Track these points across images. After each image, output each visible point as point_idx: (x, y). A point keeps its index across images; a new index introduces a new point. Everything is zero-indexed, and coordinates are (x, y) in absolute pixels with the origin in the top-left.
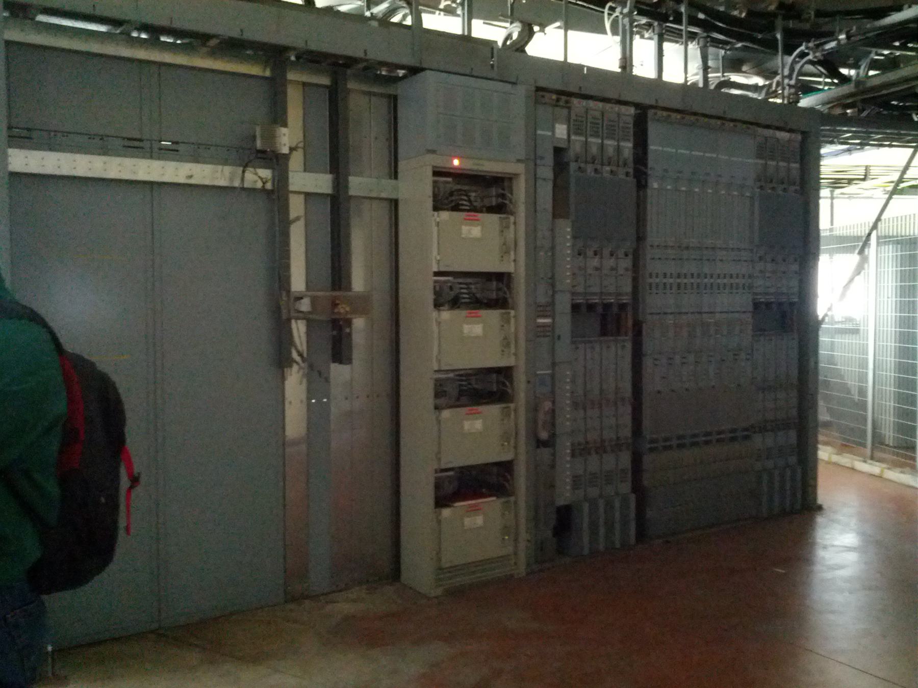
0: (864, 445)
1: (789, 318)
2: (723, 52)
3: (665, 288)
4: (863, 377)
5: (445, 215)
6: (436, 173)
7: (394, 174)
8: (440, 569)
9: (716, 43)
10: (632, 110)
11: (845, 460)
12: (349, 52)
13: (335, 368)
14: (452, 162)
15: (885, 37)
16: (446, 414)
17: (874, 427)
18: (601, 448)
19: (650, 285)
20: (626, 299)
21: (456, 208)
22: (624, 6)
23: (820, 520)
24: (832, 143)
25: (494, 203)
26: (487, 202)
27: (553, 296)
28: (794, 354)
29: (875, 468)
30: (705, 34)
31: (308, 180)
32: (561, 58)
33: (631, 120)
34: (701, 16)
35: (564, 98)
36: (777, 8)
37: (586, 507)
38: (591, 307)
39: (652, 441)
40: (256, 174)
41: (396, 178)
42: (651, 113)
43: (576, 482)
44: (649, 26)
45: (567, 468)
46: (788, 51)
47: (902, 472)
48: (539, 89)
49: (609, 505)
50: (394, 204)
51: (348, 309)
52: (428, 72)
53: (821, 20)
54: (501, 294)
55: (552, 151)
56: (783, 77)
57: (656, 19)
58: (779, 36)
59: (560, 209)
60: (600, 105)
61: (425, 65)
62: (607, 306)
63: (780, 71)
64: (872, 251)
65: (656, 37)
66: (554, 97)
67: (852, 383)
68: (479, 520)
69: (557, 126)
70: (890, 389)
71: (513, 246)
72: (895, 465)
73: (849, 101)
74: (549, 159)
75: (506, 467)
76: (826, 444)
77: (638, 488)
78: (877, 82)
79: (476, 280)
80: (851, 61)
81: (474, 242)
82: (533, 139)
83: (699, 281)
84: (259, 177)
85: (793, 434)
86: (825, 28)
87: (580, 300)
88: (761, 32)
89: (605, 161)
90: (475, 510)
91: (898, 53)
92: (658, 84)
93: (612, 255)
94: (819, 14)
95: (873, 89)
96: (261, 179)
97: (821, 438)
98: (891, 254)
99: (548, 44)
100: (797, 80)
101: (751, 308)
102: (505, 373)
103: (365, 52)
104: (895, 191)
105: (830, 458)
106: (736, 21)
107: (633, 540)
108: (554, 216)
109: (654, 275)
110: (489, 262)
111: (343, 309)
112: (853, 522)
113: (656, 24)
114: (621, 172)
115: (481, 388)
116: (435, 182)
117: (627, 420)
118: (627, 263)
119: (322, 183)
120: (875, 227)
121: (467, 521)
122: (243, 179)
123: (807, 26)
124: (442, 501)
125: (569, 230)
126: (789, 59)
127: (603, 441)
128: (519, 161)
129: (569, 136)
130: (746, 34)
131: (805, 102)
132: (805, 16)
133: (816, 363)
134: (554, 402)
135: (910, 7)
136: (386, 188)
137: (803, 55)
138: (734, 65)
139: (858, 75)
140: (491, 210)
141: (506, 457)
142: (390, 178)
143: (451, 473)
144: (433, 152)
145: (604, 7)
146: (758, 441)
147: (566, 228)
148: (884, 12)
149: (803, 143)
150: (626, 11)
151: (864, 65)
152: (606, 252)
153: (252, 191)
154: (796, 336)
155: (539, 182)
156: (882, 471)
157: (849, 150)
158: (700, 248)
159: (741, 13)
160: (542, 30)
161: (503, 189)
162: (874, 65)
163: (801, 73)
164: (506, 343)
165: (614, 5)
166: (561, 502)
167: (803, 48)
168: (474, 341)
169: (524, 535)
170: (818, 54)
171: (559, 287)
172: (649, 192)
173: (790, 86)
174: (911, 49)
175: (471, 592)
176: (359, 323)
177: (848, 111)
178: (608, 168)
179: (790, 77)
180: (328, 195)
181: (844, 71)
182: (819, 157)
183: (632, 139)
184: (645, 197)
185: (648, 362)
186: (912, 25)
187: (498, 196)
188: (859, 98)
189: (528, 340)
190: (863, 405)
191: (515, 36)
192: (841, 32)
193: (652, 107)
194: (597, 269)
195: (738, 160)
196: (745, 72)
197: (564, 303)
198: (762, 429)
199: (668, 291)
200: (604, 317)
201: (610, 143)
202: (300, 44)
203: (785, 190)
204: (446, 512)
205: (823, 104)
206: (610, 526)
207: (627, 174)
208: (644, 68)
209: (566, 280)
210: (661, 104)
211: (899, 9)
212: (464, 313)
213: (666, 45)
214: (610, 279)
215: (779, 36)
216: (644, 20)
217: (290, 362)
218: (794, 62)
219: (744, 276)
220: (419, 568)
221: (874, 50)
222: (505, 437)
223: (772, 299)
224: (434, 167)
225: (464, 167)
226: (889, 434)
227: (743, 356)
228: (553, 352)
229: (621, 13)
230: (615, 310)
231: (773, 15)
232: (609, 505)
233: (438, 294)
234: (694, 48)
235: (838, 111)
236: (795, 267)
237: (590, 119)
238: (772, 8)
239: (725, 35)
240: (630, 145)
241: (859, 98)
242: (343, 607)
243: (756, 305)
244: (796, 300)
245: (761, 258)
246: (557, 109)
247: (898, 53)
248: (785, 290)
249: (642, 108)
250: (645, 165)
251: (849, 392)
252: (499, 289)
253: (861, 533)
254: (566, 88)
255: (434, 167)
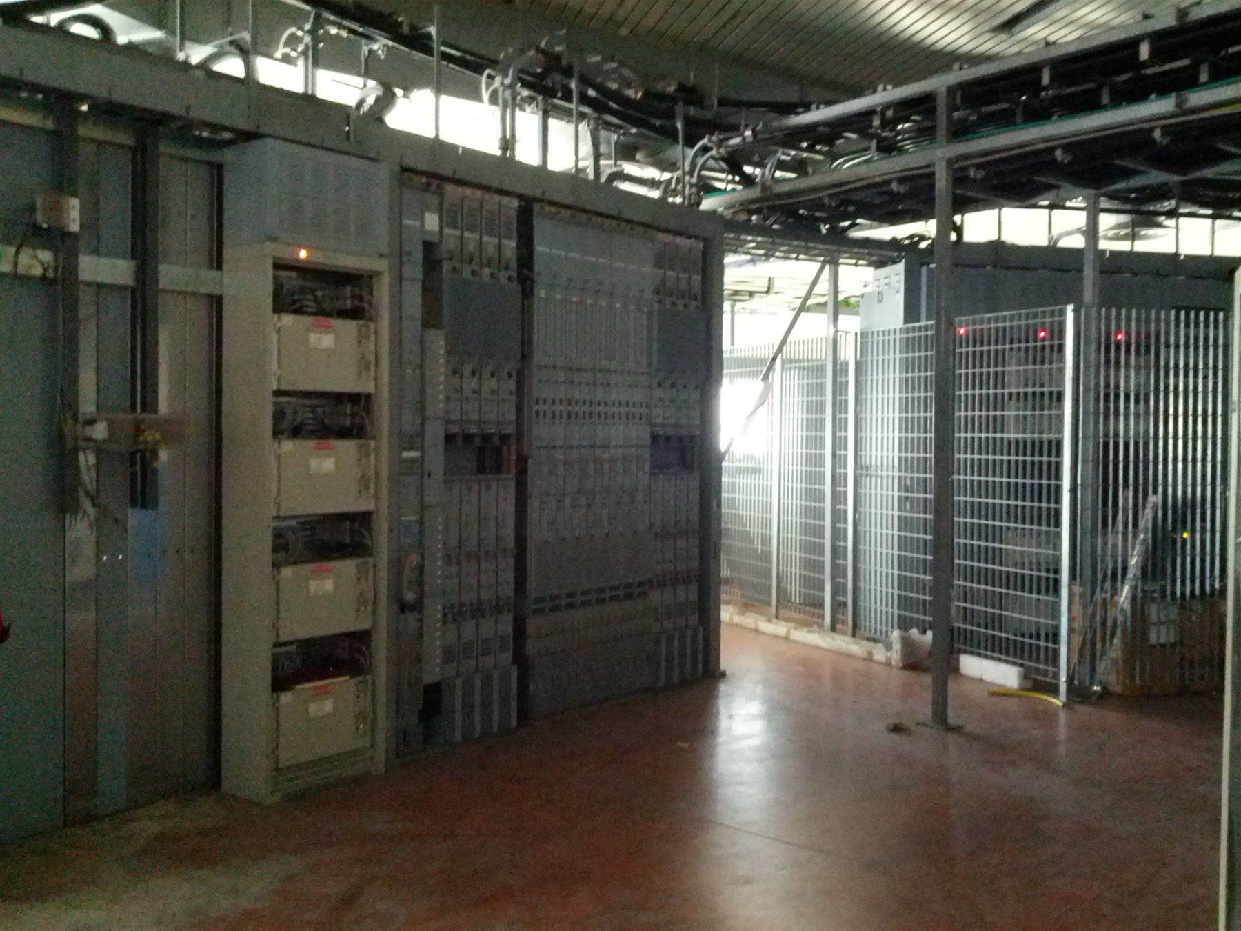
0: (769, 604)
1: (688, 454)
2: (615, 137)
3: (569, 417)
4: (767, 524)
5: (287, 320)
6: (277, 266)
7: (217, 262)
8: (277, 769)
9: (608, 126)
10: (515, 203)
11: (749, 620)
12: (161, 106)
13: (135, 518)
14: (298, 254)
15: (792, 137)
16: (287, 572)
17: (778, 582)
18: (477, 611)
19: (538, 412)
20: (510, 430)
21: (298, 311)
22: (506, 75)
23: (723, 688)
24: (735, 252)
25: (349, 307)
26: (338, 304)
27: (422, 424)
28: (695, 496)
29: (780, 628)
30: (595, 115)
31: (105, 268)
32: (431, 135)
33: (513, 214)
34: (591, 93)
35: (435, 182)
36: (677, 90)
37: (459, 683)
38: (468, 438)
39: (536, 601)
40: (35, 257)
41: (219, 267)
42: (536, 207)
43: (449, 655)
44: (531, 99)
45: (437, 639)
46: (690, 141)
47: (809, 632)
48: (405, 169)
49: (487, 679)
50: (216, 303)
51: (158, 436)
52: (269, 141)
53: (724, 110)
54: (357, 420)
55: (421, 247)
56: (684, 174)
57: (540, 93)
58: (679, 125)
59: (431, 319)
60: (478, 193)
61: (263, 130)
62: (487, 438)
63: (679, 164)
64: (776, 377)
65: (540, 113)
66: (424, 180)
67: (755, 531)
68: (328, 706)
69: (427, 215)
70: (796, 536)
71: (373, 363)
72: (801, 624)
73: (754, 207)
74: (418, 256)
75: (361, 638)
76: (728, 603)
77: (520, 658)
78: (785, 188)
79: (325, 401)
80: (756, 158)
81: (325, 354)
82: (398, 232)
83: (606, 409)
84: (35, 261)
85: (694, 587)
86: (732, 120)
87: (455, 429)
88: (660, 118)
89: (484, 262)
90: (321, 693)
91: (805, 155)
92: (541, 172)
93: (493, 375)
94: (723, 102)
95: (780, 196)
96: (42, 263)
97: (724, 597)
98: (897, 396)
99: (417, 113)
100: (699, 176)
101: (648, 442)
102: (363, 519)
103: (188, 109)
104: (803, 308)
105: (731, 619)
106: (627, 102)
107: (514, 723)
108: (425, 325)
109: (541, 401)
110: (344, 380)
111: (151, 436)
112: (759, 690)
113: (540, 98)
114: (503, 276)
115: (329, 538)
116: (275, 277)
117: (510, 576)
118: (512, 385)
119: (119, 271)
120: (780, 350)
121: (312, 708)
122: (16, 264)
123: (708, 115)
124: (280, 684)
125: (442, 343)
126: (691, 153)
127: (480, 603)
128: (381, 256)
129: (441, 228)
130: (644, 118)
131: (707, 204)
132: (706, 103)
133: (719, 506)
134: (422, 556)
135: (818, 108)
136: (208, 280)
137: (705, 149)
138: (627, 152)
139: (763, 174)
140: (344, 314)
141: (366, 625)
142: (211, 268)
143: (294, 648)
144: (273, 239)
145: (481, 73)
146: (655, 597)
147: (438, 342)
148: (789, 108)
149: (705, 254)
150: (507, 81)
151: (770, 163)
152: (467, 369)
153: (26, 279)
154: (697, 475)
155: (404, 282)
156: (788, 632)
157: (752, 261)
158: (593, 370)
159: (637, 93)
160: (405, 96)
161: (361, 288)
162: (781, 165)
163: (704, 167)
164: (363, 483)
165: (493, 73)
166: (428, 679)
167: (705, 141)
168: (324, 476)
169: (382, 722)
170: (722, 150)
171: (429, 412)
172: (536, 299)
173: (692, 185)
174: (819, 152)
175: (319, 796)
176: (163, 455)
177: (754, 217)
178: (487, 271)
179: (691, 173)
180: (125, 288)
181: (748, 169)
182: (721, 268)
183: (515, 234)
184: (531, 306)
185: (534, 504)
186: (821, 129)
187: (354, 297)
188: (766, 204)
189: (390, 479)
190: (766, 557)
191: (371, 100)
192: (746, 126)
193: (536, 200)
194: (474, 392)
195: (634, 267)
196: (638, 162)
197: (435, 432)
198: (661, 583)
199: (557, 420)
200: (481, 450)
201: (490, 241)
202: (101, 92)
203: (685, 306)
204: (286, 698)
205: (728, 207)
206: (486, 705)
207: (510, 279)
208: (527, 153)
209: (437, 405)
210: (548, 196)
211: (807, 108)
212: (312, 443)
213: (552, 122)
214: (490, 406)
215: (679, 125)
216: (525, 93)
217: (76, 508)
218: (696, 156)
219: (561, 401)
220: (249, 769)
221: (781, 150)
222: (362, 600)
223: (672, 432)
224: (275, 258)
225: (314, 259)
226: (795, 589)
227: (640, 497)
228: (421, 493)
229: (502, 84)
230: (496, 440)
231: (672, 99)
232: (487, 679)
233: (279, 415)
234: (584, 128)
235: (743, 217)
236: (695, 395)
237: (466, 209)
238: (671, 89)
239: (619, 118)
240: (513, 244)
241: (766, 204)
242: (146, 826)
243: (655, 438)
244: (698, 433)
245: (659, 385)
246: (427, 196)
247: (805, 155)
248: (683, 422)
249: (529, 202)
250: (531, 269)
251: (752, 541)
252: (353, 415)
253: (767, 701)
254: (434, 171)
255: (275, 258)
